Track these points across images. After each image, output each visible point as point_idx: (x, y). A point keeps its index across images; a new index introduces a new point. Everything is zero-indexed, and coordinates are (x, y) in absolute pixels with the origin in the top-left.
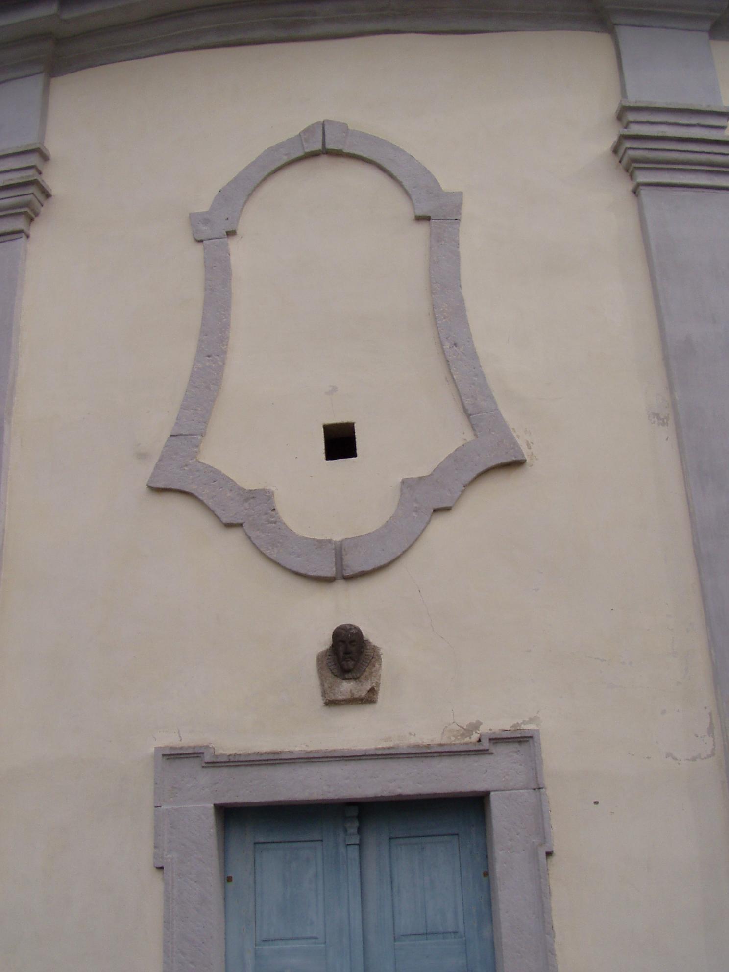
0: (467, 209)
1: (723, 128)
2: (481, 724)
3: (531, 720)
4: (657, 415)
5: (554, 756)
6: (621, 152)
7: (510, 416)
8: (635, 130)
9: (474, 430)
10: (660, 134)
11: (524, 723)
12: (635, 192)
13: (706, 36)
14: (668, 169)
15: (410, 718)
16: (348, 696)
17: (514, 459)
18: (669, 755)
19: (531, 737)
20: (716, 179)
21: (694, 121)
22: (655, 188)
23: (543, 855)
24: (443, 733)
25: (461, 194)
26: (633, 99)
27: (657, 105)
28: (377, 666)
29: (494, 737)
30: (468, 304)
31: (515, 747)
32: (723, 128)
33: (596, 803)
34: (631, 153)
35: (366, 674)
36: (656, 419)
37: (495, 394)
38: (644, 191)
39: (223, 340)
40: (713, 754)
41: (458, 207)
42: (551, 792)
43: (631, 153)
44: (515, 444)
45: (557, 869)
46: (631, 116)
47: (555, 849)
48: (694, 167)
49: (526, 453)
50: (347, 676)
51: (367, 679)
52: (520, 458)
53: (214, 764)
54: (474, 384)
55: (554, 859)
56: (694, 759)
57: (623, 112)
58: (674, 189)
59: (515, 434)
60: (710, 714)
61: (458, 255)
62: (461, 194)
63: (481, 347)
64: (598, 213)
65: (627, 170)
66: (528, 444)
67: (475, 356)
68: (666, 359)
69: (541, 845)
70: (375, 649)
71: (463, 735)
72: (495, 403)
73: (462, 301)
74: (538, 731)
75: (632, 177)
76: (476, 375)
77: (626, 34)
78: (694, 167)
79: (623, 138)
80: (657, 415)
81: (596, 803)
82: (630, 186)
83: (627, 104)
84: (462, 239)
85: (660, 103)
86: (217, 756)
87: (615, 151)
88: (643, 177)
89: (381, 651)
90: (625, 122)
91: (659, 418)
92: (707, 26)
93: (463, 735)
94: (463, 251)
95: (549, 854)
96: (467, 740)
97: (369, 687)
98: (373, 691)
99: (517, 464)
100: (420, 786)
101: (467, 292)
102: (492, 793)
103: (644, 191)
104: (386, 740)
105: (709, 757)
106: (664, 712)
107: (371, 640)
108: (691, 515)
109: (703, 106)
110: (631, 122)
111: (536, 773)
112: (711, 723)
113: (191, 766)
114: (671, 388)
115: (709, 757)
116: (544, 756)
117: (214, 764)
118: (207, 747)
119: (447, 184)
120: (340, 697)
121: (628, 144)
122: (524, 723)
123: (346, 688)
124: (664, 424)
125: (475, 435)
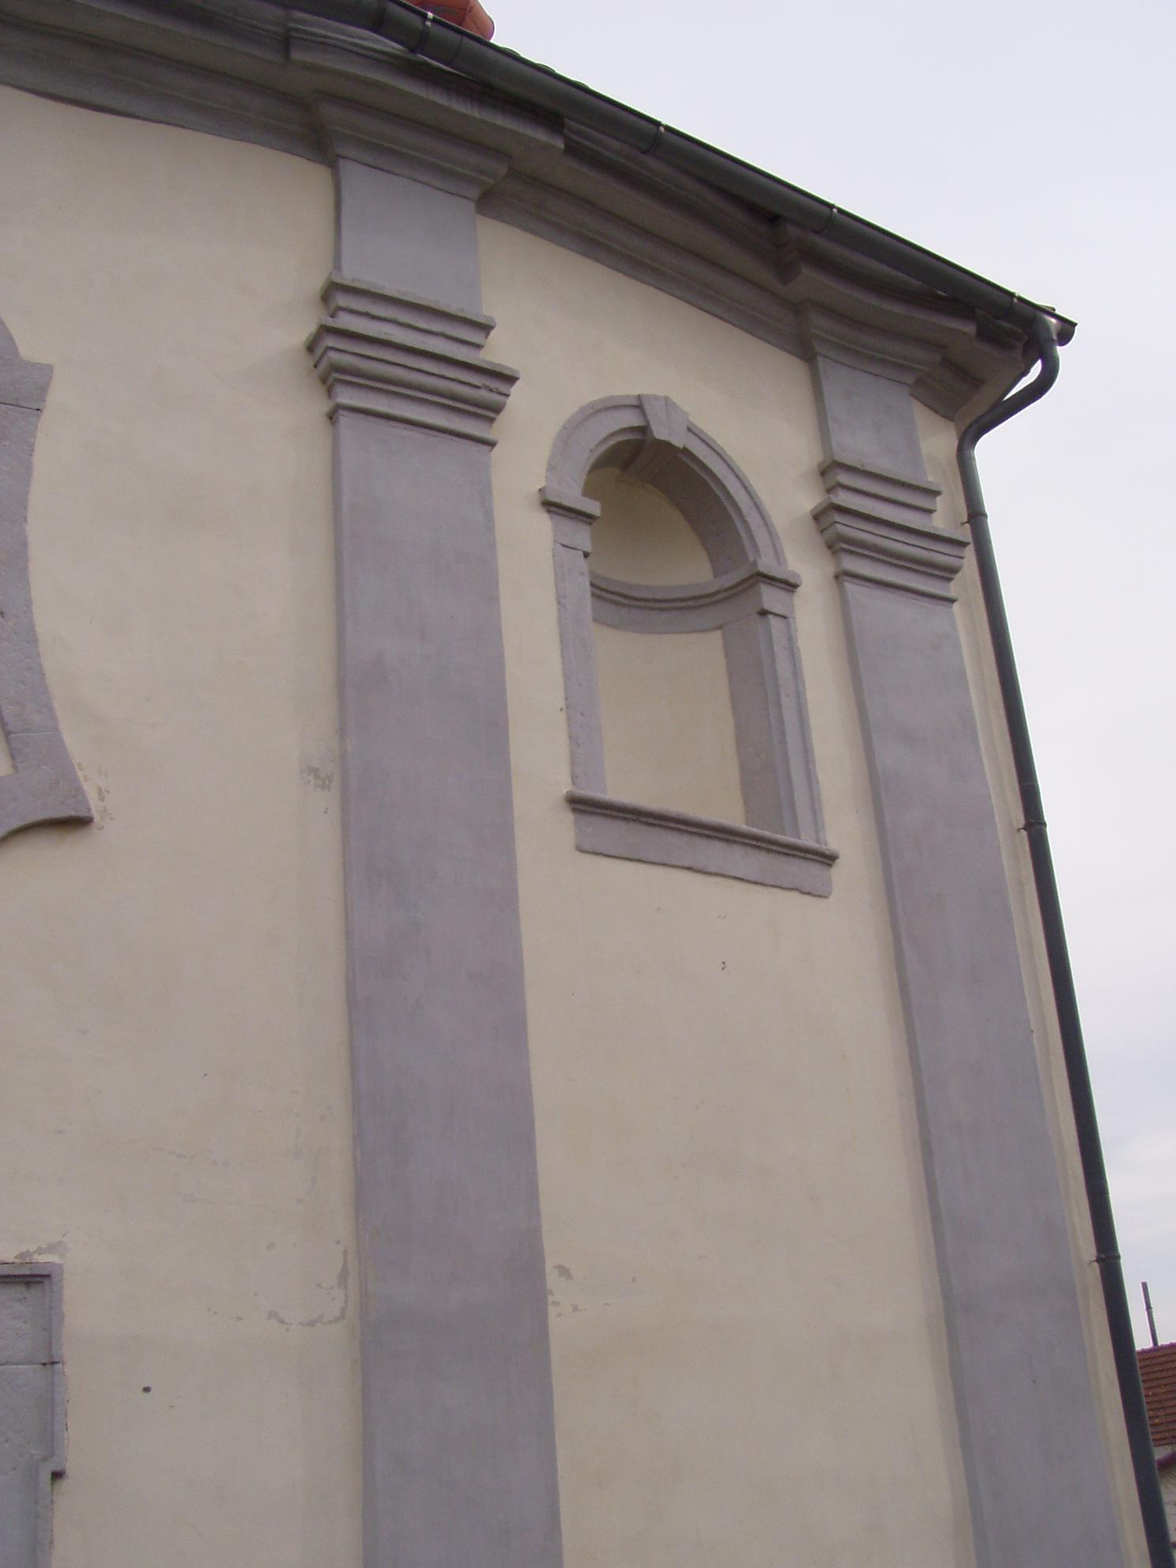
0: (58, 395)
1: (479, 347)
4: (314, 771)
5: (86, 1310)
6: (319, 351)
7: (76, 743)
8: (345, 322)
9: (13, 757)
10: (383, 337)
11: (39, 1251)
12: (332, 417)
13: (472, 206)
14: (372, 389)
17: (73, 813)
18: (272, 1315)
19: (48, 1276)
20: (812, 695)
21: (437, 326)
22: (362, 416)
23: (45, 1477)
25: (50, 369)
26: (349, 275)
27: (386, 292)
30: (35, 550)
31: (19, 1291)
32: (479, 347)
33: (147, 1390)
34: (334, 356)
36: (311, 778)
37: (57, 706)
38: (344, 419)
40: (342, 1316)
41: (43, 390)
42: (73, 1369)
43: (334, 356)
44: (79, 790)
45: (69, 1500)
46: (342, 300)
47: (70, 1468)
48: (425, 396)
49: (95, 807)
52: (83, 813)
54: (23, 682)
55: (64, 1485)
56: (312, 1323)
57: (332, 289)
58: (392, 423)
59: (80, 774)
60: (345, 1253)
61: (29, 468)
62: (50, 369)
63: (46, 623)
64: (269, 439)
65: (324, 380)
66: (100, 791)
67: (31, 638)
68: (341, 686)
69: (45, 1459)
70: (22, 1255)
72: (54, 718)
73: (24, 544)
74: (60, 1266)
75: (330, 392)
76: (30, 669)
77: (356, 176)
78: (425, 396)
79: (325, 330)
80: (314, 771)
81: (147, 1390)
82: (326, 406)
83: (339, 281)
84: (41, 442)
85: (391, 289)
87: (311, 348)
88: (347, 397)
90: (333, 306)
91: (317, 776)
92: (475, 193)
94: (39, 461)
95: (57, 1476)
99: (78, 823)
101: (36, 530)
103: (344, 419)
105: (336, 1320)
106: (271, 1246)
108: (349, 934)
109: (453, 308)
110: (342, 309)
111: (50, 1337)
112: (345, 1267)
114: (342, 731)
115: (336, 1320)
116: (67, 1308)
119: (31, 347)
121: (331, 341)
122: (39, 1251)
124: (324, 787)
125: (15, 767)
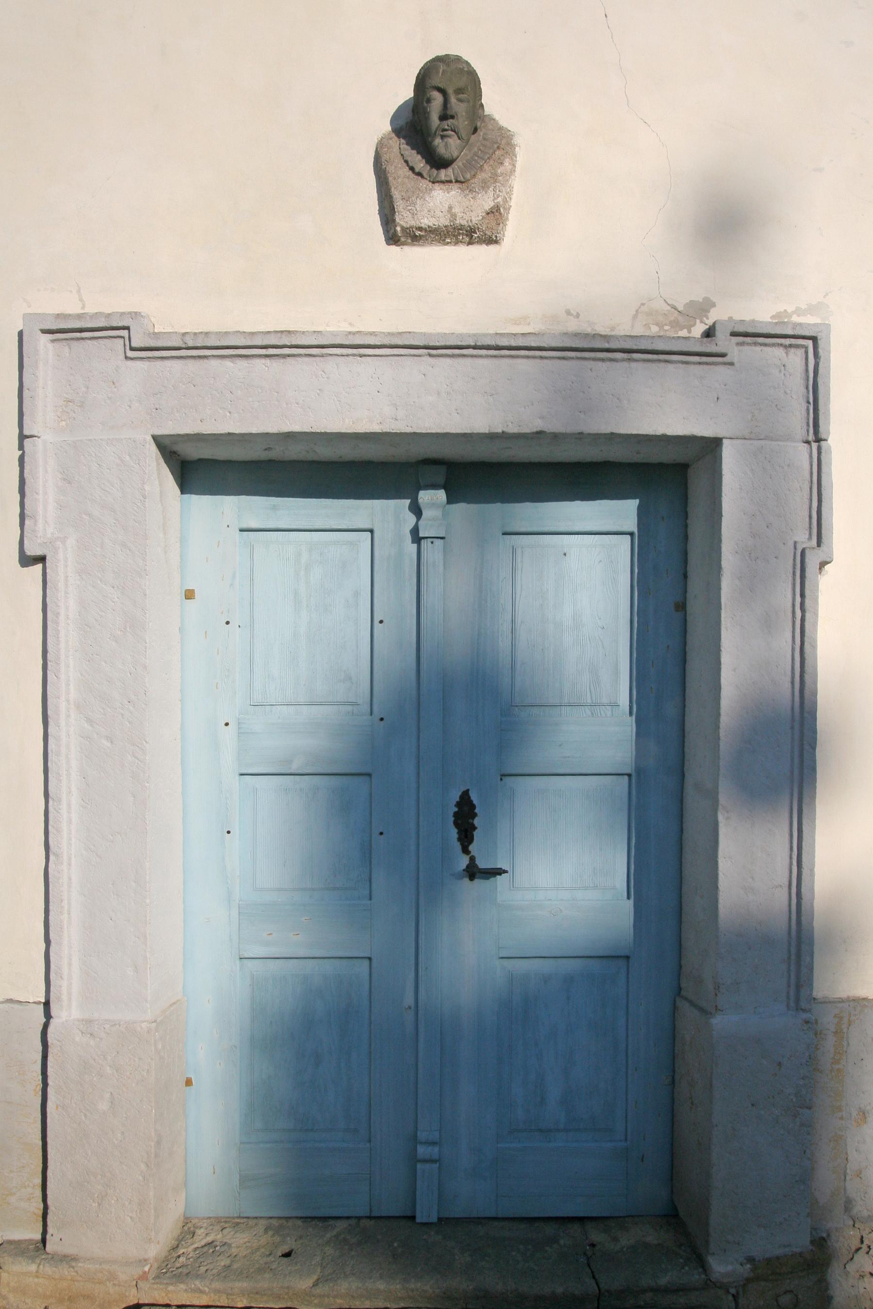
2: (713, 305)
3: (812, 309)
15: (579, 236)
16: (443, 221)
24: (635, 317)
28: (507, 163)
29: (741, 329)
35: (481, 176)
39: (386, 178)
50: (443, 174)
51: (485, 186)
53: (154, 350)
71: (675, 325)
86: (156, 335)
89: (516, 140)
93: (675, 325)
96: (684, 333)
97: (489, 204)
98: (496, 213)
100: (339, 1301)
102: (724, 441)
104: (516, 323)
107: (497, 117)
113: (107, 354)
117: (154, 350)
118: (136, 315)
120: (426, 222)
122: (798, 311)
123: (438, 203)
